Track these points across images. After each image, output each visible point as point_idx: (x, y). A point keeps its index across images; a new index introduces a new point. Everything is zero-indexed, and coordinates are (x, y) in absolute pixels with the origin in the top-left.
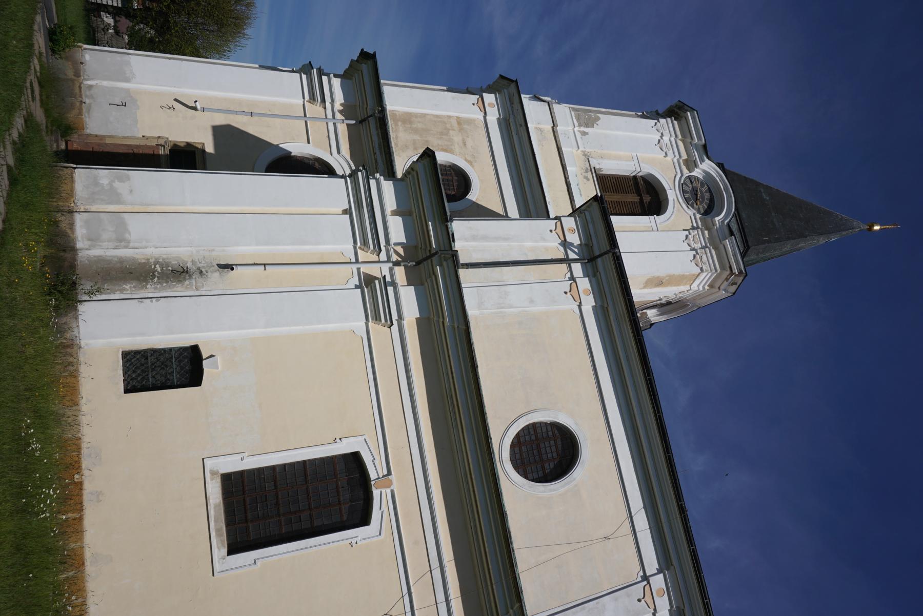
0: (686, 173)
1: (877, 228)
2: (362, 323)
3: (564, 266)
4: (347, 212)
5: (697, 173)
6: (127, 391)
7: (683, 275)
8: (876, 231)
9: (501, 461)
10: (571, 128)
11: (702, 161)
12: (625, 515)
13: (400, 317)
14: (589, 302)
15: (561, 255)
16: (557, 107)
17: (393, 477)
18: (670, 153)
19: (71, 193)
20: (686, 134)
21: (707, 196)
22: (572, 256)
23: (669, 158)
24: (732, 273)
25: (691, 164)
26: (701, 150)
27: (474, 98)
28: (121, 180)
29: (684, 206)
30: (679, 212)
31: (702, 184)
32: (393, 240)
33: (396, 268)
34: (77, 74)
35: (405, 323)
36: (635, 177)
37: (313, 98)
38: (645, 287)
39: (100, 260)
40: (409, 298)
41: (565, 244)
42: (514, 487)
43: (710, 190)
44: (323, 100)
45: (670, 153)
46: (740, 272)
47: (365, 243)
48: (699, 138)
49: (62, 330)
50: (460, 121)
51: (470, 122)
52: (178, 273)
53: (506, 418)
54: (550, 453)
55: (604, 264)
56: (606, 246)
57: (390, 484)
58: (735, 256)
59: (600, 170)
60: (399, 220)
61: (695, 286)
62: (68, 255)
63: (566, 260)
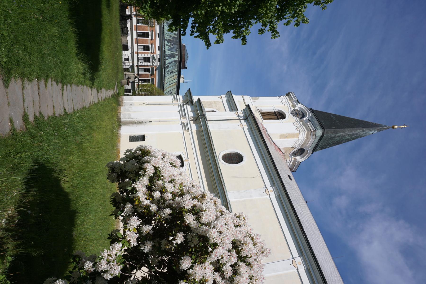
0: (293, 109)
1: (396, 127)
2: (181, 131)
3: (239, 121)
4: (179, 111)
5: (296, 108)
6: (130, 141)
7: (293, 134)
8: (396, 128)
9: (219, 159)
10: (250, 101)
11: (297, 104)
12: (259, 173)
13: (191, 129)
14: (246, 128)
15: (238, 118)
16: (244, 97)
17: (189, 159)
18: (286, 104)
19: (121, 110)
20: (291, 99)
21: (302, 114)
22: (240, 118)
23: (286, 105)
24: (311, 131)
25: (294, 106)
26: (297, 102)
27: (219, 96)
28: (130, 108)
29: (292, 117)
30: (290, 119)
31: (299, 111)
32: (190, 116)
33: (191, 121)
34: (122, 100)
35: (193, 131)
36: (275, 112)
37: (175, 100)
38: (280, 138)
39: (125, 121)
40: (194, 127)
41: (239, 116)
42: (223, 166)
43: (302, 112)
44: (177, 99)
45: (286, 104)
46: (314, 130)
47: (183, 116)
48: (295, 99)
49: (118, 110)
50: (214, 102)
51: (218, 101)
52: (141, 123)
53: (220, 151)
54: (235, 158)
55: (250, 119)
56: (249, 113)
57: (188, 161)
58: (311, 127)
59: (261, 110)
60: (192, 113)
61: (300, 138)
62: (119, 114)
63: (240, 119)
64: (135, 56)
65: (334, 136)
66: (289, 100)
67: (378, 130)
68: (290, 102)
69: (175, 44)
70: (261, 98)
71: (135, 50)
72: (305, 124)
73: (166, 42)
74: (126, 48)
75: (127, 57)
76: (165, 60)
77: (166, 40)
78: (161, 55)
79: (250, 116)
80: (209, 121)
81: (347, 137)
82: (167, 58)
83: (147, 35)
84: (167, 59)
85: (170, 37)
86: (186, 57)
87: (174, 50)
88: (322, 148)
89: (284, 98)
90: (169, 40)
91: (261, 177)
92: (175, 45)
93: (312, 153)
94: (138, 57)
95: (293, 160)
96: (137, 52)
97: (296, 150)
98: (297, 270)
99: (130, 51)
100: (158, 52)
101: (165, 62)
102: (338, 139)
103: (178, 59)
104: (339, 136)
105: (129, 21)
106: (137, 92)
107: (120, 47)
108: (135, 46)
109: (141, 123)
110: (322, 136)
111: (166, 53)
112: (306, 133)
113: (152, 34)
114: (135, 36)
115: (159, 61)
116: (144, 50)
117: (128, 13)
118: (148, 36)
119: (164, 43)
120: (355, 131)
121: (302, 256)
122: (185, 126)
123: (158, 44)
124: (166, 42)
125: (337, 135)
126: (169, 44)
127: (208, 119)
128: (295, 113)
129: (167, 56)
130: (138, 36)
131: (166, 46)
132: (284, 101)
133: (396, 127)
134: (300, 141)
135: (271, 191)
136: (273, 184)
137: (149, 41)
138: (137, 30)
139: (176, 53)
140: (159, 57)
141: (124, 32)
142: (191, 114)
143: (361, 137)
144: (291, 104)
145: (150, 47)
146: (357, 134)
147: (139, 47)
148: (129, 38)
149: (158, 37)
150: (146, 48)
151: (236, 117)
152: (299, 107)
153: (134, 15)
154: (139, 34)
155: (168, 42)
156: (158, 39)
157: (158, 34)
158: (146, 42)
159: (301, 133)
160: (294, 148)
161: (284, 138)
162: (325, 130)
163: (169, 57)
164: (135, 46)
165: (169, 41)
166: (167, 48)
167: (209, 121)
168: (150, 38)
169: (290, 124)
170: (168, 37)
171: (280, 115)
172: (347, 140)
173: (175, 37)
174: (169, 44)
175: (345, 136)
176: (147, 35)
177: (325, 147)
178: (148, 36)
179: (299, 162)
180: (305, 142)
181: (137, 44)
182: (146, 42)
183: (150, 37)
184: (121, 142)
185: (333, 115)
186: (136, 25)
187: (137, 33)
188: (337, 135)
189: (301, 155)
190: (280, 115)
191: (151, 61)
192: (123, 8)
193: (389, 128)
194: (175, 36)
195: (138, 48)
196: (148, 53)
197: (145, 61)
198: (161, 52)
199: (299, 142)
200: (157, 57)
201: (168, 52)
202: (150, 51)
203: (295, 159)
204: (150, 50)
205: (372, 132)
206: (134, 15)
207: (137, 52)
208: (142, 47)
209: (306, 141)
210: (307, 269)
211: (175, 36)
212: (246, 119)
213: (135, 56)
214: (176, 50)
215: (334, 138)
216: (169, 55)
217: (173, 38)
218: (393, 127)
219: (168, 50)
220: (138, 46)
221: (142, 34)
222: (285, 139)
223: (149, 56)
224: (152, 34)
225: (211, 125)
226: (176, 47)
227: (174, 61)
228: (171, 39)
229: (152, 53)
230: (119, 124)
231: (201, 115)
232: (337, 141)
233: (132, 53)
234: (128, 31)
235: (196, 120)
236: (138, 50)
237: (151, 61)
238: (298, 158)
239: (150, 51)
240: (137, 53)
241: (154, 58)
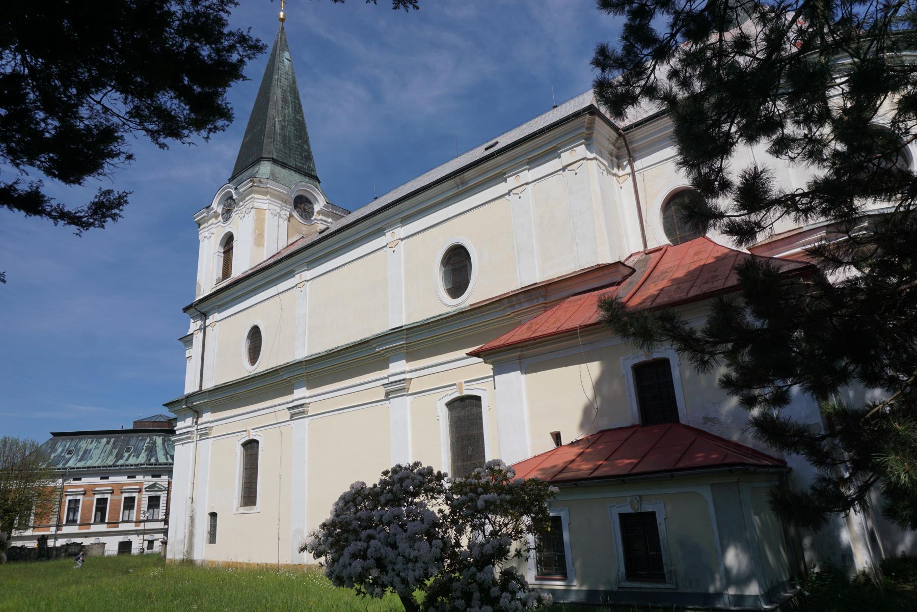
0: (220, 218)
1: (282, 14)
12: (277, 297)
25: (216, 215)
35: (211, 419)
38: (263, 245)
42: (266, 362)
52: (192, 519)
61: (265, 206)
63: (205, 328)
64: (141, 527)
65: (279, 138)
66: (206, 225)
67: (282, 50)
68: (210, 222)
69: (128, 444)
70: (198, 280)
71: (131, 527)
72: (243, 197)
73: (120, 462)
74: (125, 547)
75: (146, 544)
76: (156, 464)
77: (116, 461)
78: (145, 472)
79: (198, 308)
80: (201, 386)
81: (289, 110)
82: (153, 460)
83: (102, 503)
84: (157, 460)
85: (111, 452)
86: (162, 420)
87: (141, 444)
88: (309, 158)
89: (203, 233)
90: (116, 456)
91: (281, 296)
92: (131, 443)
93: (316, 178)
94: (148, 521)
95: (320, 217)
96: (136, 522)
97: (295, 214)
98: (402, 240)
99: (132, 538)
100: (139, 478)
101: (161, 464)
102: (291, 129)
103: (159, 436)
104: (283, 128)
105: (50, 543)
106: (161, 525)
107: (124, 557)
108: (122, 527)
109: (192, 519)
110: (275, 161)
111: (143, 462)
112: (256, 196)
113: (100, 492)
114: (103, 528)
115: (159, 476)
116: (132, 507)
117: (33, 544)
118: (77, 501)
119: (122, 466)
120: (277, 94)
121: (385, 229)
122: (204, 434)
123: (123, 479)
124: (120, 462)
125: (278, 130)
126: (126, 455)
127: (197, 389)
128: (227, 213)
129: (150, 460)
130: (102, 521)
131: (128, 463)
132: (206, 234)
133: (282, 14)
134: (271, 207)
135: (301, 278)
136: (290, 274)
137: (115, 497)
138: (90, 524)
139: (148, 440)
140: (149, 478)
141: (73, 551)
142: (189, 421)
143: (294, 82)
144: (213, 220)
145: (126, 495)
146: (284, 92)
147: (126, 519)
148: (86, 542)
149: (107, 478)
150: (129, 503)
151: (201, 335)
152: (217, 206)
153: (57, 530)
154: (98, 520)
155: (122, 457)
156: (113, 479)
157: (102, 478)
158: (115, 505)
159: (256, 205)
160: (291, 216)
161: (263, 237)
162: (264, 155)
163: (152, 457)
164: (122, 527)
165: (119, 456)
166: (132, 460)
167: (201, 386)
168: (108, 496)
169: (241, 225)
170: (110, 457)
171: (228, 241)
172: (298, 108)
173: (114, 443)
174: (126, 455)
175: (284, 116)
176: (102, 503)
177: (305, 154)
178: (77, 501)
179: (325, 206)
180: (277, 196)
181: (119, 523)
182: (115, 505)
183: (106, 496)
184: (240, 560)
185: (245, 136)
186: (80, 525)
187: (95, 523)
188: (278, 130)
189: (310, 202)
190: (228, 241)
191: (158, 493)
192: (20, 555)
193: (283, 29)
194: (112, 442)
195: (129, 521)
196: (140, 500)
197: (158, 506)
198: (140, 473)
199: (275, 208)
200: (148, 480)
201: (142, 459)
202: (135, 495)
203: (319, 213)
204: (134, 495)
205: (286, 61)
206: (57, 530)
207: (136, 522)
208: (127, 512)
209: (273, 195)
210: (401, 222)
211: (112, 442)
212: (204, 316)
213: (141, 527)
214: (142, 440)
215: (284, 136)
216: (147, 456)
217: (114, 447)
218: (282, 20)
219: (138, 457)
220: (123, 522)
221: (99, 514)
222: (266, 237)
223: (145, 496)
224: (100, 492)
225: (208, 385)
226: (134, 440)
227: (163, 444)
228: (115, 451)
229: (140, 491)
230: (188, 562)
231: (186, 403)
232: (296, 130)
233: (137, 533)
234: (74, 544)
235: (196, 412)
236: (132, 521)
237: (158, 493)
238: (317, 208)
239: (135, 495)
240: (138, 522)
241: (151, 488)
